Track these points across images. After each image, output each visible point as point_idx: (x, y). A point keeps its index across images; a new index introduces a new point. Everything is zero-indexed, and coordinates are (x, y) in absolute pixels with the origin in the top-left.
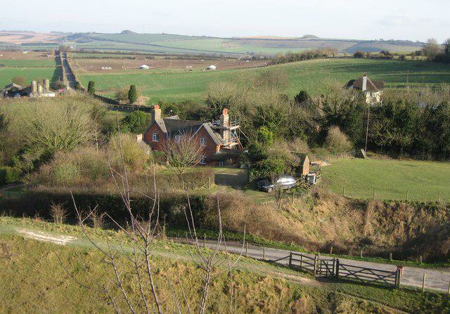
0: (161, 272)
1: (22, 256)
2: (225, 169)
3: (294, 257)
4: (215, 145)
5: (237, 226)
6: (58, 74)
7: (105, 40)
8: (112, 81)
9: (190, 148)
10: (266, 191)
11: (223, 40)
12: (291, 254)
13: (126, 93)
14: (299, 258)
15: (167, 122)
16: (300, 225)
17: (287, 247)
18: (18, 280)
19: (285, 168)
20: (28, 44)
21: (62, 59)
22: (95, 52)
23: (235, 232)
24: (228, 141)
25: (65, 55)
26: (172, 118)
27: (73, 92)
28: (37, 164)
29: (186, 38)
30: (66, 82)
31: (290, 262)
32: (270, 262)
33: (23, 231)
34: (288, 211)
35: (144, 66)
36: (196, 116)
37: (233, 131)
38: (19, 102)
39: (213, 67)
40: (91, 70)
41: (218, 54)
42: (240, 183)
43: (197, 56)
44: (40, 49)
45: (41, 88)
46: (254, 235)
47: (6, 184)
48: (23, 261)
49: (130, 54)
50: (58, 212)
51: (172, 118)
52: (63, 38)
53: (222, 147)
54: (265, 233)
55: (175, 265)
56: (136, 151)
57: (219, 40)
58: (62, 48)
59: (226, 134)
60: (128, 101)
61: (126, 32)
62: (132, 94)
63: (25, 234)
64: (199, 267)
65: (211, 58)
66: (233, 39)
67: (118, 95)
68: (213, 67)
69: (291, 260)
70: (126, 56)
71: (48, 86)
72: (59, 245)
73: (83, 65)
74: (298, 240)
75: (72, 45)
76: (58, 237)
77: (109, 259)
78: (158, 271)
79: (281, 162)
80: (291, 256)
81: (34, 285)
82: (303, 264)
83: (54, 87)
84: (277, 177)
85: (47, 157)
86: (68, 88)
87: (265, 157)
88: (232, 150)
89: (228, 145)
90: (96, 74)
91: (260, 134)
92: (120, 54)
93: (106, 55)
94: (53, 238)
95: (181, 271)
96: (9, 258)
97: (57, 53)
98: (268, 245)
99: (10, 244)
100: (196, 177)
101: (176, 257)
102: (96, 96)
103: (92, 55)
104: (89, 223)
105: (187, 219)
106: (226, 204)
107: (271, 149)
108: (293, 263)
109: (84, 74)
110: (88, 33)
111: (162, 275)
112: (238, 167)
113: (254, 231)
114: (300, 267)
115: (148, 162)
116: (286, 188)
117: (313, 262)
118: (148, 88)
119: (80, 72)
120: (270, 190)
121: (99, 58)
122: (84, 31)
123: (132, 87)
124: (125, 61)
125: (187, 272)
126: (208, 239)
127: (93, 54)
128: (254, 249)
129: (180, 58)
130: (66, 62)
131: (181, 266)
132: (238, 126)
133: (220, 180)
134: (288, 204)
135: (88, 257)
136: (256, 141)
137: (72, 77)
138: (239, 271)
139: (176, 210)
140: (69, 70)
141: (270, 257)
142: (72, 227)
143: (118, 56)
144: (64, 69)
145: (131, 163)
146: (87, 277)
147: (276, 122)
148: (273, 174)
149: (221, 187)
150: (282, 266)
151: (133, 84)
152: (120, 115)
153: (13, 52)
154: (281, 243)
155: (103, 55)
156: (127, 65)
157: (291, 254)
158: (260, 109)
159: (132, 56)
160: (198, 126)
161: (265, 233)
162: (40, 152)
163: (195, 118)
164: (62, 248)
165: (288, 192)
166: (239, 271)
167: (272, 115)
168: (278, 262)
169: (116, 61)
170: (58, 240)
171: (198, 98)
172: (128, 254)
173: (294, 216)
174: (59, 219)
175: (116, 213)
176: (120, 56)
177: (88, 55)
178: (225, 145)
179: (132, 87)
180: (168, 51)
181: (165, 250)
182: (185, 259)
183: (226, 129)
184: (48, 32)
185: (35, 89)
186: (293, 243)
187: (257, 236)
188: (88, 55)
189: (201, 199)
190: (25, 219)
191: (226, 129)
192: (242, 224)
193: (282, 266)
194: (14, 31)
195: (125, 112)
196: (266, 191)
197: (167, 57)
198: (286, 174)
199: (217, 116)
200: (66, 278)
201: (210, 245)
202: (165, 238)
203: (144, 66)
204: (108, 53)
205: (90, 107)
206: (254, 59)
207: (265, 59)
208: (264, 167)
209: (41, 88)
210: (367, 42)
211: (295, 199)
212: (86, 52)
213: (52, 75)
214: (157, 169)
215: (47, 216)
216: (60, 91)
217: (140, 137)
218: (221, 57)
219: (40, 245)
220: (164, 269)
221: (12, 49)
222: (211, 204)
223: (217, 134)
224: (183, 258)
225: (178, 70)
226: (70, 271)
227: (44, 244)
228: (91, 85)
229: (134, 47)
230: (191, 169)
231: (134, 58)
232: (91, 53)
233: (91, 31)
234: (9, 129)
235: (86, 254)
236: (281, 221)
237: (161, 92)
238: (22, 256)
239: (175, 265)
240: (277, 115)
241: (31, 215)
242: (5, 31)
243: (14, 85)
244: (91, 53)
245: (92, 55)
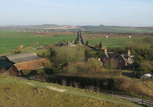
0: (94, 104)
1: (47, 95)
2: (127, 71)
3: (144, 101)
4: (125, 62)
5: (125, 90)
6: (78, 39)
7: (94, 28)
8: (94, 41)
9: (114, 63)
10: (140, 78)
11: (135, 28)
12: (143, 100)
13: (99, 45)
14: (145, 102)
15: (109, 54)
16: (151, 91)
17: (143, 98)
18: (45, 103)
19: (148, 70)
20: (69, 30)
21: (80, 34)
22: (91, 32)
23: (125, 91)
24: (130, 61)
25: (81, 33)
26: (111, 53)
27: (82, 45)
28: (62, 67)
29: (122, 27)
30: (80, 42)
31: (142, 103)
32: (135, 103)
33: (49, 87)
34: (147, 86)
35: (107, 37)
36: (121, 52)
37: (132, 57)
38: (63, 48)
39: (130, 37)
40: (88, 38)
41: (133, 33)
42: (131, 76)
43: (125, 33)
44: (73, 31)
45: (71, 43)
46: (131, 93)
47: (53, 73)
48: (47, 97)
49: (102, 33)
50: (64, 82)
51: (111, 53)
52: (80, 28)
53: (127, 63)
54: (135, 92)
55: (99, 102)
56: (97, 63)
57: (133, 28)
58: (80, 31)
59: (129, 59)
60: (99, 48)
61: (101, 25)
62: (100, 45)
63: (49, 88)
64: (108, 103)
65: (130, 34)
66: (138, 27)
67: (96, 46)
68: (130, 37)
69: (143, 102)
70: (100, 33)
71: (73, 43)
72: (60, 92)
73: (86, 36)
74: (148, 96)
75: (83, 30)
76: (61, 90)
77: (76, 98)
78: (93, 103)
79: (146, 68)
80: (143, 101)
81: (50, 105)
82: (147, 104)
83: (75, 43)
84: (144, 74)
85: (66, 65)
86: (80, 43)
87: (140, 66)
88: (131, 64)
89: (130, 63)
90: (90, 39)
91: (139, 58)
92: (99, 32)
93: (94, 33)
94: (58, 90)
95: (101, 104)
96: (43, 95)
97: (78, 32)
98: (136, 97)
99: (44, 91)
100: (115, 73)
101: (100, 99)
102: (89, 46)
103: (89, 33)
104: (74, 86)
105: (108, 86)
106: (121, 82)
107: (142, 64)
108: (143, 103)
109: (86, 39)
110: (89, 26)
111: (94, 105)
112: (132, 70)
113: (132, 92)
114: (146, 105)
115: (101, 67)
116: (148, 77)
117: (150, 103)
118: (107, 44)
119: (85, 38)
120: (142, 78)
121: (92, 34)
122: (88, 25)
123: (101, 43)
124: (100, 35)
125: (103, 104)
126: (114, 93)
127: (90, 33)
128: (131, 98)
129: (119, 34)
130: (81, 36)
131: (101, 102)
132: (133, 56)
133: (124, 74)
134: (147, 83)
135: (69, 97)
136: (137, 61)
137: (82, 41)
138: (122, 105)
139: (105, 84)
140: (81, 38)
141: (135, 101)
142: (67, 87)
143: (98, 33)
144: (80, 37)
145: (95, 68)
146: (68, 103)
147: (147, 55)
148: (141, 72)
149: (124, 76)
150: (139, 104)
151: (100, 42)
152: (95, 52)
153: (64, 32)
154: (141, 96)
155: (93, 33)
156: (100, 36)
157: (143, 100)
158: (142, 50)
159: (102, 33)
160: (119, 56)
161: (135, 92)
162: (64, 63)
163: (118, 54)
164: (61, 93)
165: (148, 79)
166: (122, 105)
167: (146, 52)
168: (138, 103)
169: (98, 35)
170: (60, 90)
171: (122, 47)
172: (83, 97)
173: (149, 87)
174: (64, 84)
175: (84, 83)
176: (99, 33)
177: (88, 33)
178: (129, 62)
179: (101, 43)
180: (115, 32)
181: (97, 96)
182: (103, 99)
183: (129, 57)
184: (76, 25)
185: (69, 44)
186: (145, 97)
187: (132, 93)
188: (88, 33)
189: (113, 79)
190: (52, 83)
191: (129, 57)
192: (128, 89)
193: (139, 104)
194: (65, 25)
195: (97, 51)
196: (140, 78)
197: (115, 33)
198: (148, 73)
199: (127, 53)
200: (61, 103)
201: (114, 96)
202: (99, 92)
203: (107, 37)
204: (95, 32)
205: (85, 49)
206: (145, 34)
207: (149, 34)
208: (140, 70)
209: (71, 43)
210: (126, 27)
211: (150, 82)
212: (88, 32)
213: (75, 40)
214: (104, 70)
215: (60, 83)
216: (78, 44)
217: (99, 59)
218: (134, 34)
219: (54, 92)
220: (95, 103)
221: (64, 31)
222: (116, 81)
223: (126, 58)
224: (103, 99)
225: (118, 38)
226: (62, 101)
227: (55, 91)
228: (87, 42)
229: (104, 30)
230: (113, 70)
231: (103, 34)
232: (89, 32)
233: (90, 25)
234: (57, 55)
235: (69, 96)
236: (144, 90)
237: (111, 45)
238: (47, 95)
239: (99, 102)
240: (147, 52)
241: (54, 82)
242: (62, 25)
243: (63, 42)
244: (89, 32)
245: (89, 33)
